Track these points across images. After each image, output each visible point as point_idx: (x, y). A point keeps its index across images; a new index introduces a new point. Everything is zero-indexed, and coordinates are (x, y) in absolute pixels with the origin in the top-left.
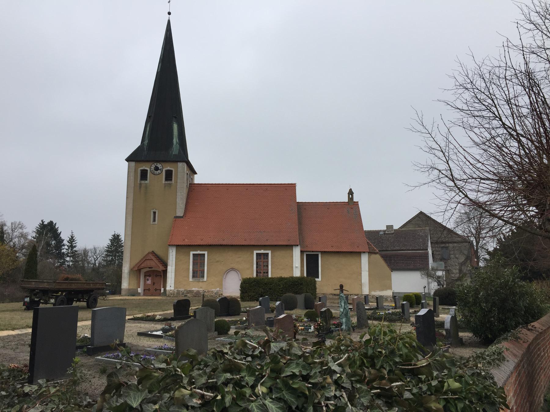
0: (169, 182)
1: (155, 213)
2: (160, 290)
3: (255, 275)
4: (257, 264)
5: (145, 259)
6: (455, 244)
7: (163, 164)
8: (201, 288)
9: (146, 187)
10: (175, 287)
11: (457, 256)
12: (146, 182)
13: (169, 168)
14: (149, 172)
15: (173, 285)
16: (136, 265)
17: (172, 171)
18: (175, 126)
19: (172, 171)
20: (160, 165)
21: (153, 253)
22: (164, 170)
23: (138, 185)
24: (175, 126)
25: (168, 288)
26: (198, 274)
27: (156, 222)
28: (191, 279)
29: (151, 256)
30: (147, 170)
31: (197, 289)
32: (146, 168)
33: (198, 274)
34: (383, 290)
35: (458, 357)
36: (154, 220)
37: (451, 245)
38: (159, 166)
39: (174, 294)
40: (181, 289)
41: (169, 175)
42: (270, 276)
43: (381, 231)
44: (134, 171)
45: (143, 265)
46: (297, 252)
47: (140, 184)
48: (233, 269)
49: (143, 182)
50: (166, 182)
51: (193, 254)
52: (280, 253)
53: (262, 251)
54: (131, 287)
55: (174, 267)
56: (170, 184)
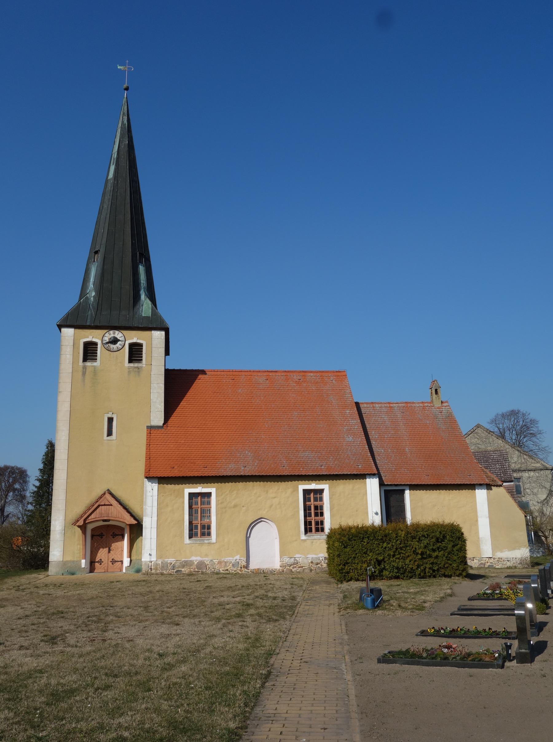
0: (136, 365)
1: (110, 420)
2: (122, 562)
3: (154, 559)
4: (190, 507)
5: (95, 506)
6: (532, 474)
7: (125, 332)
8: (206, 555)
9: (95, 371)
10: (159, 556)
11: (535, 491)
12: (95, 364)
13: (135, 340)
14: (99, 346)
15: (154, 553)
16: (82, 517)
17: (141, 345)
18: (142, 269)
19: (141, 345)
20: (120, 335)
21: (108, 490)
22: (127, 343)
23: (81, 369)
24: (142, 269)
25: (145, 558)
26: (199, 529)
27: (114, 436)
28: (187, 540)
29: (108, 496)
30: (96, 344)
31: (199, 559)
32: (94, 340)
33: (199, 529)
34: (514, 549)
35: (240, 586)
36: (110, 433)
37: (526, 475)
38: (118, 334)
39: (156, 569)
40: (170, 560)
41: (135, 353)
42: (409, 518)
43: (52, 485)
44: (72, 344)
45: (93, 516)
46: (372, 484)
47: (85, 368)
48: (259, 520)
49: (88, 364)
50: (132, 365)
51: (190, 494)
52: (345, 487)
53: (313, 486)
54: (68, 558)
55: (155, 518)
56: (138, 368)
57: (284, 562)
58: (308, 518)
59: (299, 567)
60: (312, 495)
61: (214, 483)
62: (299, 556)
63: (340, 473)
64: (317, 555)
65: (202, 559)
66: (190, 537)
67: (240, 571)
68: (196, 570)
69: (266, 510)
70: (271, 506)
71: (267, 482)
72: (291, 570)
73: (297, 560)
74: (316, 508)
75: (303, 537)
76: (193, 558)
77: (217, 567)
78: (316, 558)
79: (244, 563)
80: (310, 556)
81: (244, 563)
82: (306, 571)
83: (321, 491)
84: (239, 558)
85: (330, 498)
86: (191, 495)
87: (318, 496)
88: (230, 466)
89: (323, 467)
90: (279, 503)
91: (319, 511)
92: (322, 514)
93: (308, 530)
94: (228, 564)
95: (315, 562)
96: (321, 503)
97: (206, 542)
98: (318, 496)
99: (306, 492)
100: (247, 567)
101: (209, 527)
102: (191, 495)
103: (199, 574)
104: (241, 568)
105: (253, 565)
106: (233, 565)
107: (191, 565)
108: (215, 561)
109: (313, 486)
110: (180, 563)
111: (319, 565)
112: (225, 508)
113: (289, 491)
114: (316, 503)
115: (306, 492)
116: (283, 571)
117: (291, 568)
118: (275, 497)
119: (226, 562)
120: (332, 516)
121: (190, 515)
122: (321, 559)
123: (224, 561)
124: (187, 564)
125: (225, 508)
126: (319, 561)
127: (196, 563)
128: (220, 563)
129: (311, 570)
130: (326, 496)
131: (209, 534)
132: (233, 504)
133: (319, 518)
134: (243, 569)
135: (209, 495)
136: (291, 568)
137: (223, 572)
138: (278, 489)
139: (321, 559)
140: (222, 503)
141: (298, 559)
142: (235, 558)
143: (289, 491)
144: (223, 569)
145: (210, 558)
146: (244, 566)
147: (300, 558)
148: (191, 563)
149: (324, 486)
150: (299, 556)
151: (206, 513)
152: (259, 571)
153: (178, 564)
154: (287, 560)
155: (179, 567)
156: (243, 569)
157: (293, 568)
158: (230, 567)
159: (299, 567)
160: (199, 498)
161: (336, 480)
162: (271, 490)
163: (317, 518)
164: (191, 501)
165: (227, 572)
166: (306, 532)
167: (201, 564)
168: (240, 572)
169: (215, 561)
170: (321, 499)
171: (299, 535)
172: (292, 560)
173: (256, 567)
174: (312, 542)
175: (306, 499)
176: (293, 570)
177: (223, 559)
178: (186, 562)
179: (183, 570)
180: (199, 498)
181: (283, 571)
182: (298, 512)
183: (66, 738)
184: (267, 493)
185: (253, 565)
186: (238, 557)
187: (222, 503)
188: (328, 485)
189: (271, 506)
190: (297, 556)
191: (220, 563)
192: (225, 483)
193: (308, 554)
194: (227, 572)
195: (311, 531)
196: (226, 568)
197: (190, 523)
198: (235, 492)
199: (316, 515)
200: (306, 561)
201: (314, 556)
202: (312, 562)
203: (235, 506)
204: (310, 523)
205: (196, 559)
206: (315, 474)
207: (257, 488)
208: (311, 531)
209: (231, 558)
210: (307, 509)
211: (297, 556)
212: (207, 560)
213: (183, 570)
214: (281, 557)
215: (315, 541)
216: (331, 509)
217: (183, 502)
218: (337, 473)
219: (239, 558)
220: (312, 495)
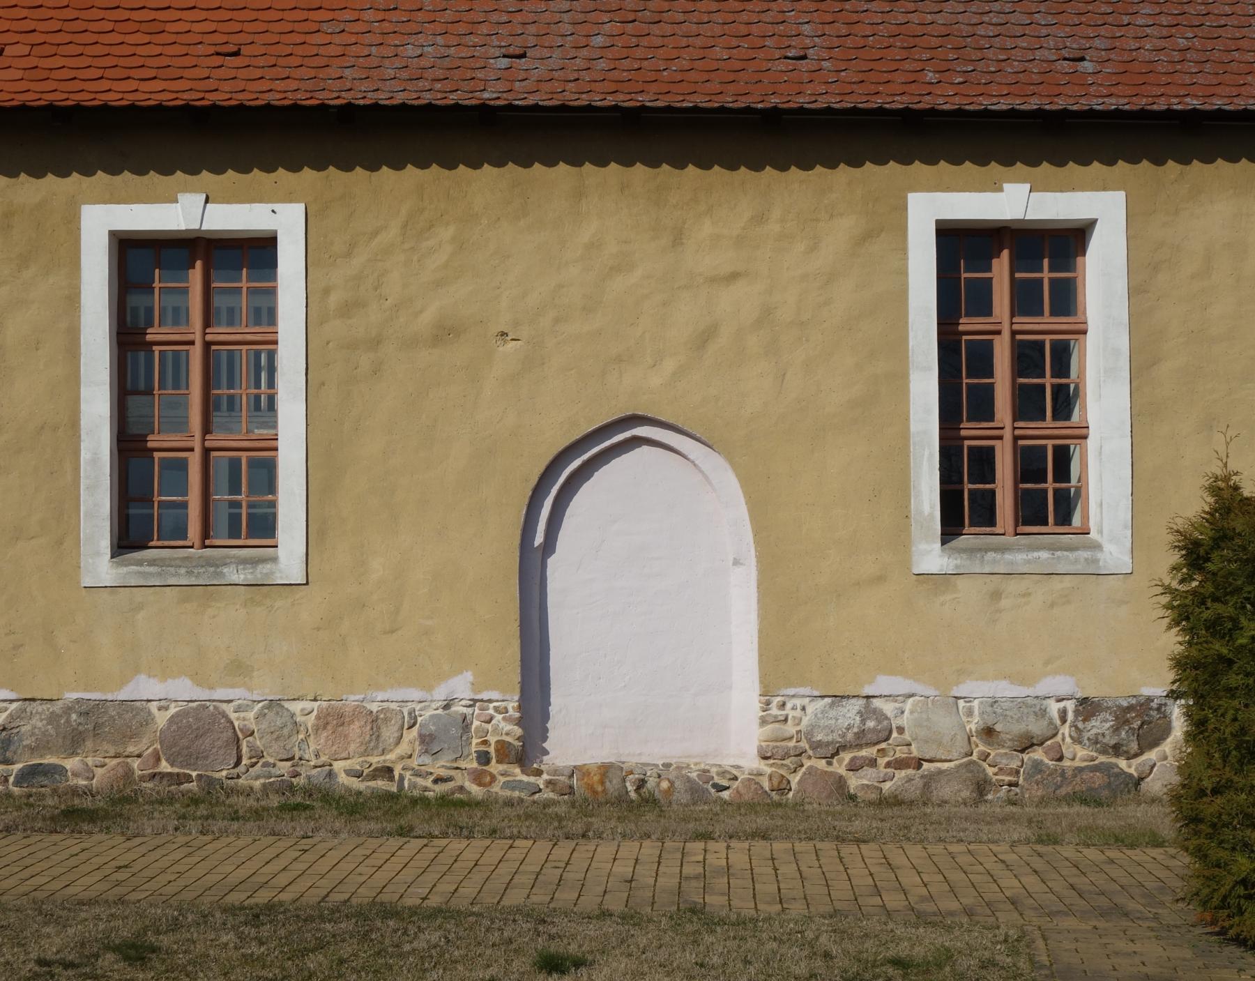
4: (129, 337)
8: (238, 670)
24: (539, 539)
26: (179, 484)
28: (98, 563)
31: (183, 690)
33: (179, 484)
53: (1012, 199)
57: (790, 729)
58: (969, 429)
59: (900, 764)
60: (1000, 270)
61: (295, 168)
62: (900, 685)
63: (1218, 103)
64: (1022, 680)
65: (202, 694)
66: (129, 537)
67: (478, 778)
68: (165, 767)
69: (669, 365)
70: (705, 337)
71: (680, 165)
72: (841, 782)
73: (880, 716)
74: (1027, 357)
75: (931, 556)
76: (145, 688)
77: (314, 749)
78: (1021, 704)
79: (506, 729)
80: (978, 690)
81: (506, 729)
82: (946, 790)
83: (1069, 240)
84: (472, 688)
85: (1136, 291)
86: (131, 252)
87: (1046, 275)
88: (410, 51)
89: (1087, 66)
90: (766, 316)
91: (1048, 381)
92: (1066, 401)
93: (962, 511)
94: (389, 733)
95: (1009, 728)
96: (1061, 323)
97: (235, 575)
98: (1046, 275)
99: (961, 244)
100: (526, 752)
101: (266, 473)
102: (131, 252)
103: (196, 786)
104: (484, 758)
105: (573, 744)
106: (426, 740)
107: (131, 734)
108: (296, 707)
109: (1012, 199)
110: (53, 718)
111: (1038, 754)
112: (375, 343)
113: (844, 227)
114: (1026, 322)
115: (961, 244)
116: (782, 787)
117: (839, 767)
118: (734, 277)
119: (375, 721)
120: (1144, 414)
121: (128, 388)
122: (1054, 708)
123: (359, 711)
124: (90, 724)
125: (375, 343)
126: (1037, 728)
127: (162, 719)
128: (333, 720)
129: (982, 787)
130: (1103, 275)
131: (264, 526)
132: (428, 317)
133: (1044, 431)
134: (495, 767)
135: (258, 251)
136: (839, 767)
137: (356, 784)
138: (760, 219)
139: (1054, 708)
140: (347, 309)
141: (888, 708)
142: (440, 693)
143: (844, 227)
144: (355, 763)
145: (264, 689)
146: (503, 747)
147: (901, 696)
148: (133, 716)
149: (1097, 203)
150: (900, 685)
151: (239, 378)
152: (612, 786)
153: (34, 725)
154: (808, 712)
155: (41, 746)
156: (495, 767)
157: (854, 767)
158: (401, 752)
159: (900, 764)
160: (196, 275)
161: (1185, 160)
162: (707, 228)
163: (1030, 427)
164: (135, 300)
165: (381, 784)
166: (952, 525)
167: (198, 728)
168: (475, 790)
169: (296, 707)
170: (1066, 298)
171: (900, 540)
172: (849, 714)
173: (594, 756)
174: (996, 595)
175: (957, 298)
176: (855, 782)
177: (353, 699)
178: (89, 710)
179: (71, 764)
180: (196, 275)
181: (782, 787)
182: (899, 380)
183: (310, 977)
184: (678, 239)
185: (573, 744)
186: (460, 686)
187: (347, 309)
188: (1121, 195)
189: (705, 337)
190: (884, 684)
191: (333, 720)
192: (373, 167)
193: (962, 674)
194: (381, 784)
195: (985, 514)
196: (376, 760)
197: (130, 445)
198: (446, 233)
199: (1028, 404)
200: (944, 723)
201: (1006, 690)
202: (988, 732)
203: (445, 332)
204: (984, 462)
205: (163, 692)
206: (1033, 104)
207: (593, 216)
208: (985, 514)
209: (415, 694)
210: (960, 362)
211: (884, 684)
212: (240, 700)
213: (71, 764)
214: (767, 693)
215: (1013, 586)
216: (1142, 366)
217: (73, 300)
218: (1193, 103)
219: (472, 688)
220: (1000, 270)
